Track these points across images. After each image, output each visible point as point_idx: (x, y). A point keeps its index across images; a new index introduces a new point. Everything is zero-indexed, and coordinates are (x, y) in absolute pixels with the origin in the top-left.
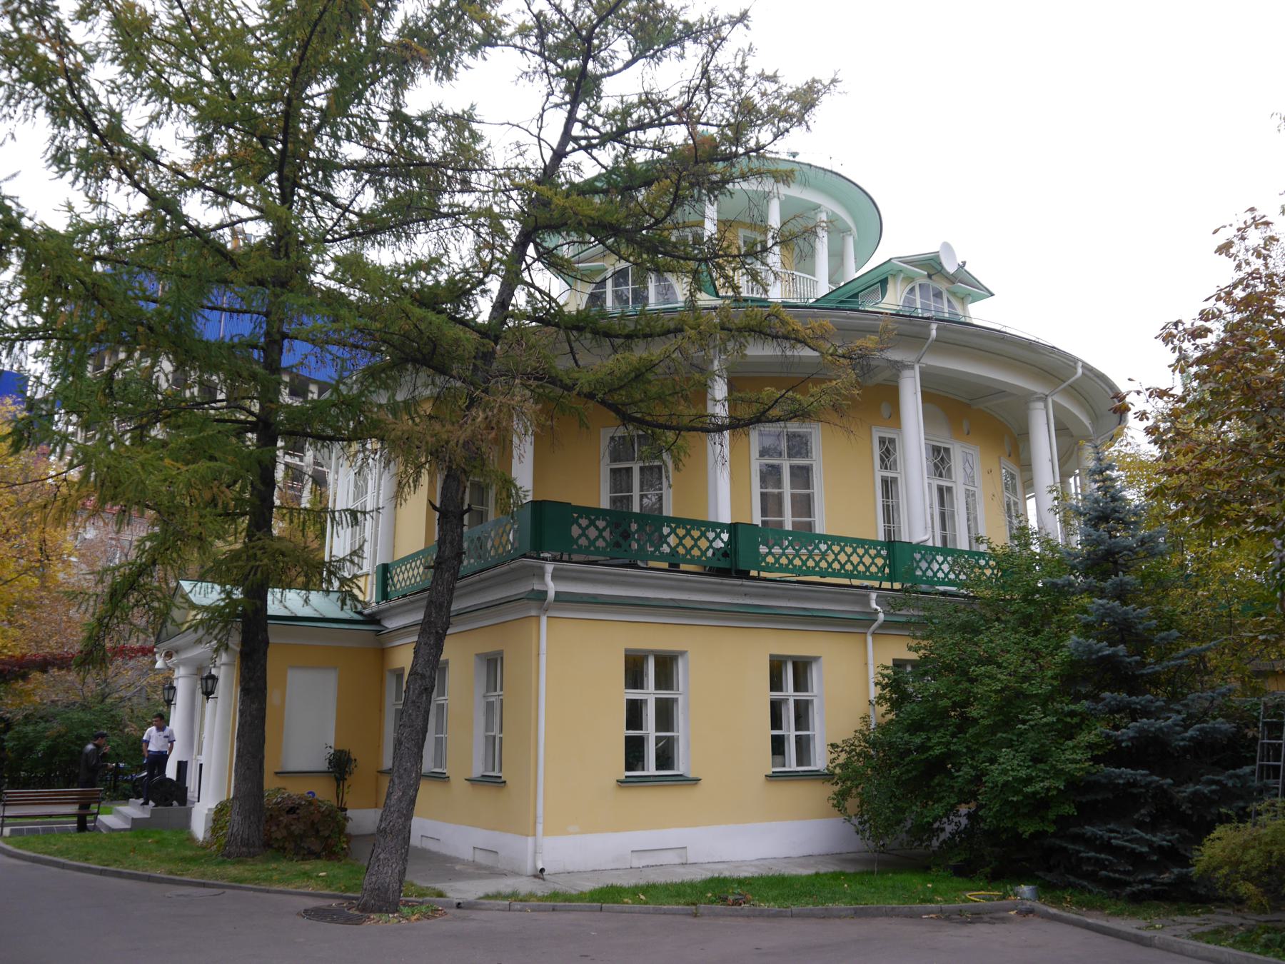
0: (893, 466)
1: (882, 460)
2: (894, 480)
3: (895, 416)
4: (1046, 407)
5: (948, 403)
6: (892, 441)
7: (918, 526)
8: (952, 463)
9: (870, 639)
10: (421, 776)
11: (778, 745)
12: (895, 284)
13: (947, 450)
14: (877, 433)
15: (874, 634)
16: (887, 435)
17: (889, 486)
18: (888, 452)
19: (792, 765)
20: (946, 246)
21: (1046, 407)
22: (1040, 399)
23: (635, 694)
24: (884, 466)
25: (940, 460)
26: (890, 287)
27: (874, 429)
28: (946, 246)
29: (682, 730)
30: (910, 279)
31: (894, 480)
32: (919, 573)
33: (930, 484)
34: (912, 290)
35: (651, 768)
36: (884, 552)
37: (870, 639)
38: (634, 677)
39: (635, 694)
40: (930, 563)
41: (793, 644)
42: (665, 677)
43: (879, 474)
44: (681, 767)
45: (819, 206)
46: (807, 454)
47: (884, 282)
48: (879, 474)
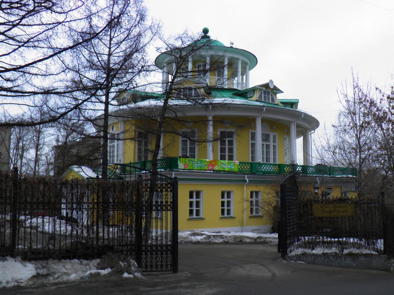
0: (254, 140)
1: (251, 138)
2: (254, 143)
3: (255, 128)
4: (294, 124)
5: (270, 124)
6: (254, 133)
7: (259, 159)
8: (270, 138)
9: (245, 187)
10: (60, 220)
11: (223, 211)
12: (257, 92)
13: (269, 135)
14: (251, 131)
15: (246, 185)
16: (253, 131)
17: (253, 145)
18: (253, 137)
19: (195, 216)
20: (271, 81)
21: (294, 124)
22: (293, 122)
23: (191, 200)
24: (252, 140)
25: (266, 138)
26: (256, 92)
27: (250, 130)
28: (271, 81)
29: (201, 208)
30: (261, 90)
31: (254, 143)
32: (258, 170)
33: (263, 145)
34: (261, 93)
35: (226, 215)
36: (250, 165)
37: (245, 187)
38: (191, 196)
39: (191, 200)
40: (261, 167)
41: (226, 188)
42: (198, 196)
43: (251, 142)
44: (201, 216)
45: (239, 58)
46: (232, 137)
47: (254, 90)
48: (251, 142)
